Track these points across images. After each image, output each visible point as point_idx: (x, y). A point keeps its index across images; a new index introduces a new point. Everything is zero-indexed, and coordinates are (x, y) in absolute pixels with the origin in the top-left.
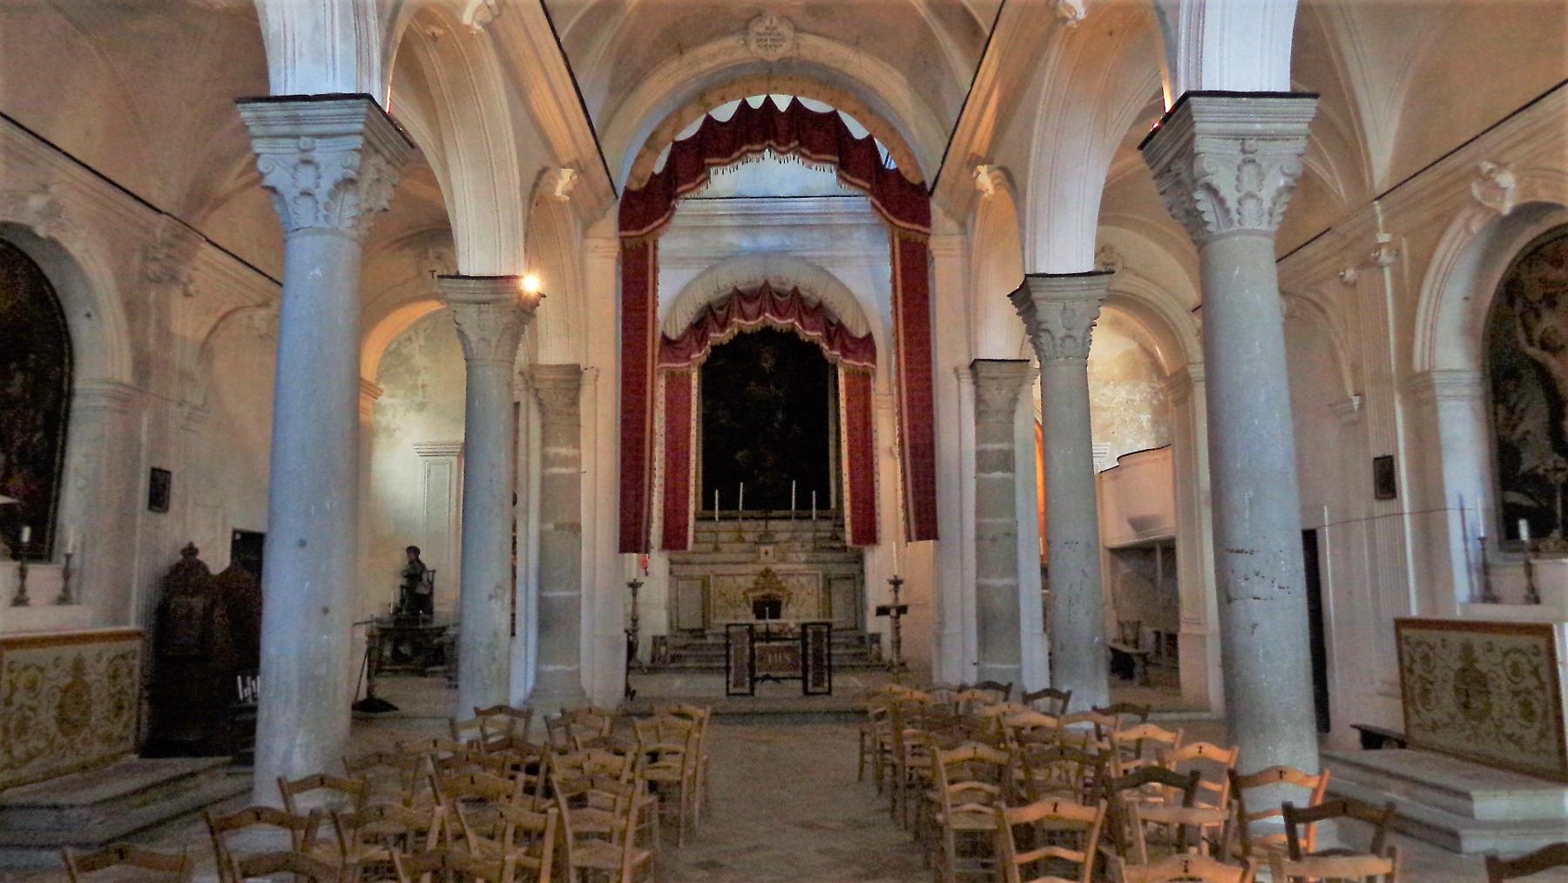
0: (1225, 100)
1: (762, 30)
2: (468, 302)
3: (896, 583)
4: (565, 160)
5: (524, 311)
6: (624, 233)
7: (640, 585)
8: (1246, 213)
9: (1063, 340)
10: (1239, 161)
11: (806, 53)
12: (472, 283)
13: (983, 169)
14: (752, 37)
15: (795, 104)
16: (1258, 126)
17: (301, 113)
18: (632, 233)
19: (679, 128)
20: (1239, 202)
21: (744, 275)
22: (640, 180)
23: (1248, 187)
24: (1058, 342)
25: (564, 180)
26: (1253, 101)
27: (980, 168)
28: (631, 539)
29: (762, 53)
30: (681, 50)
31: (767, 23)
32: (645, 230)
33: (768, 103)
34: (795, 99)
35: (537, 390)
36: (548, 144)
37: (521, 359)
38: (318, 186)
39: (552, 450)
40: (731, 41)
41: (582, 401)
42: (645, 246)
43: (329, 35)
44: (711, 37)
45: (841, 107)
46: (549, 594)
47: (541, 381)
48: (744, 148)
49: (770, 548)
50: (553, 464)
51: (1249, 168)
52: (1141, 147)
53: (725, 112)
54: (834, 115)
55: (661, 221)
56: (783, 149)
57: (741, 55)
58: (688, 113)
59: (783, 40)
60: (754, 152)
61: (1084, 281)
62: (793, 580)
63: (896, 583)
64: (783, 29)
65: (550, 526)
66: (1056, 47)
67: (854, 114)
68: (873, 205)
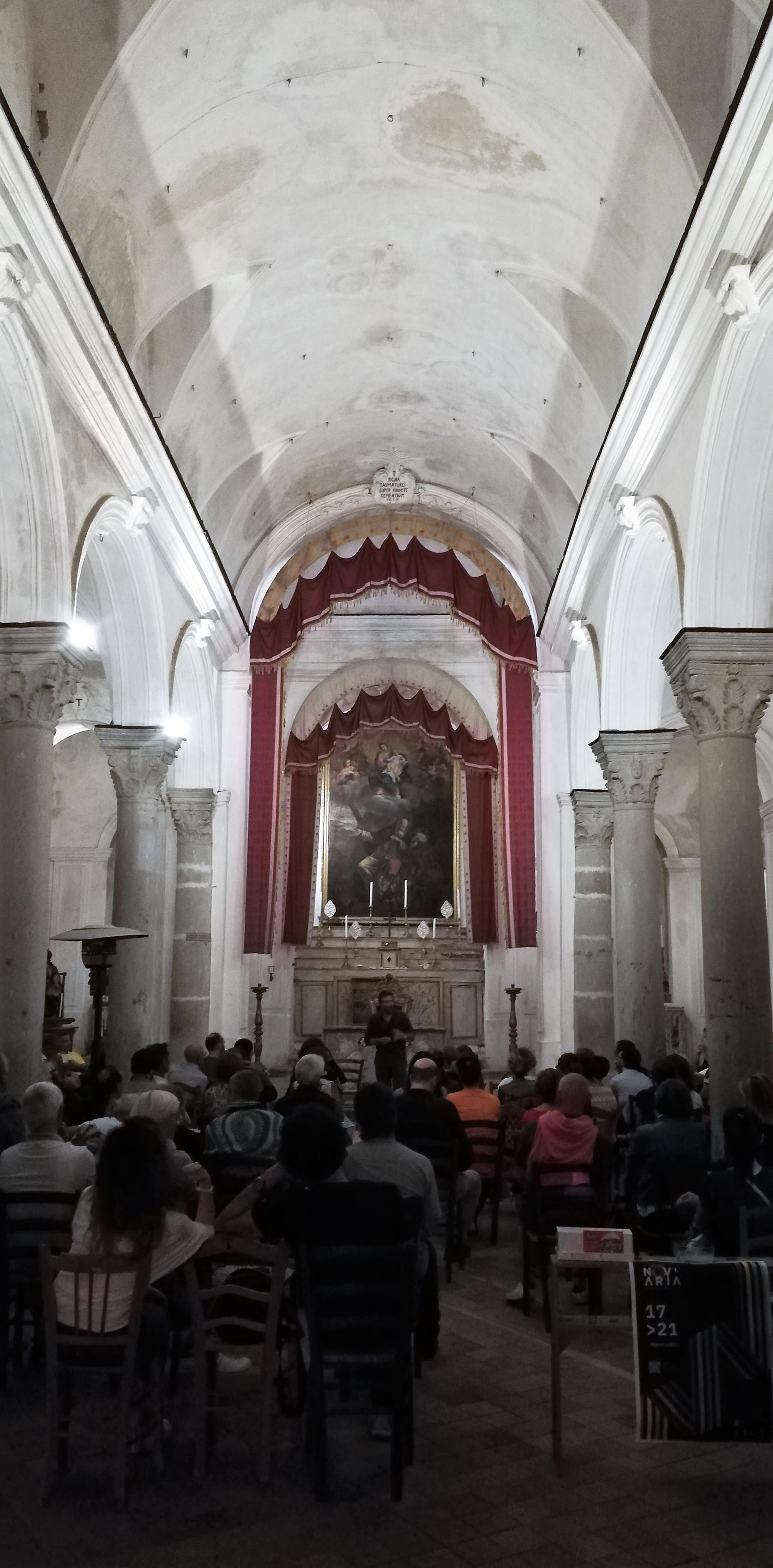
0: (714, 634)
1: (386, 481)
2: (121, 748)
3: (513, 992)
4: (203, 611)
5: (168, 754)
6: (254, 660)
7: (264, 990)
8: (731, 721)
9: (632, 787)
10: (726, 681)
11: (425, 500)
12: (124, 732)
13: (577, 624)
14: (376, 489)
15: (414, 544)
16: (740, 654)
17: (13, 636)
18: (262, 660)
19: (304, 566)
20: (726, 713)
21: (373, 679)
22: (270, 611)
23: (734, 699)
24: (628, 789)
25: (202, 630)
26: (735, 635)
27: (574, 623)
28: (254, 940)
29: (385, 501)
30: (311, 500)
31: (391, 475)
32: (274, 658)
33: (390, 542)
34: (414, 539)
35: (173, 811)
36: (189, 600)
37: (163, 789)
38: (23, 690)
39: (186, 867)
40: (357, 490)
41: (215, 822)
42: (274, 674)
43: (33, 574)
44: (340, 488)
45: (457, 547)
46: (176, 999)
47: (179, 803)
48: (368, 584)
49: (393, 955)
50: (187, 880)
51: (735, 686)
52: (661, 658)
53: (348, 551)
54: (450, 554)
55: (288, 650)
56: (404, 585)
57: (366, 501)
58: (315, 550)
59: (405, 490)
60: (377, 587)
61: (650, 737)
62: (414, 987)
63: (513, 992)
64: (406, 479)
65: (183, 936)
66: (494, 723)
67: (468, 554)
68: (483, 642)
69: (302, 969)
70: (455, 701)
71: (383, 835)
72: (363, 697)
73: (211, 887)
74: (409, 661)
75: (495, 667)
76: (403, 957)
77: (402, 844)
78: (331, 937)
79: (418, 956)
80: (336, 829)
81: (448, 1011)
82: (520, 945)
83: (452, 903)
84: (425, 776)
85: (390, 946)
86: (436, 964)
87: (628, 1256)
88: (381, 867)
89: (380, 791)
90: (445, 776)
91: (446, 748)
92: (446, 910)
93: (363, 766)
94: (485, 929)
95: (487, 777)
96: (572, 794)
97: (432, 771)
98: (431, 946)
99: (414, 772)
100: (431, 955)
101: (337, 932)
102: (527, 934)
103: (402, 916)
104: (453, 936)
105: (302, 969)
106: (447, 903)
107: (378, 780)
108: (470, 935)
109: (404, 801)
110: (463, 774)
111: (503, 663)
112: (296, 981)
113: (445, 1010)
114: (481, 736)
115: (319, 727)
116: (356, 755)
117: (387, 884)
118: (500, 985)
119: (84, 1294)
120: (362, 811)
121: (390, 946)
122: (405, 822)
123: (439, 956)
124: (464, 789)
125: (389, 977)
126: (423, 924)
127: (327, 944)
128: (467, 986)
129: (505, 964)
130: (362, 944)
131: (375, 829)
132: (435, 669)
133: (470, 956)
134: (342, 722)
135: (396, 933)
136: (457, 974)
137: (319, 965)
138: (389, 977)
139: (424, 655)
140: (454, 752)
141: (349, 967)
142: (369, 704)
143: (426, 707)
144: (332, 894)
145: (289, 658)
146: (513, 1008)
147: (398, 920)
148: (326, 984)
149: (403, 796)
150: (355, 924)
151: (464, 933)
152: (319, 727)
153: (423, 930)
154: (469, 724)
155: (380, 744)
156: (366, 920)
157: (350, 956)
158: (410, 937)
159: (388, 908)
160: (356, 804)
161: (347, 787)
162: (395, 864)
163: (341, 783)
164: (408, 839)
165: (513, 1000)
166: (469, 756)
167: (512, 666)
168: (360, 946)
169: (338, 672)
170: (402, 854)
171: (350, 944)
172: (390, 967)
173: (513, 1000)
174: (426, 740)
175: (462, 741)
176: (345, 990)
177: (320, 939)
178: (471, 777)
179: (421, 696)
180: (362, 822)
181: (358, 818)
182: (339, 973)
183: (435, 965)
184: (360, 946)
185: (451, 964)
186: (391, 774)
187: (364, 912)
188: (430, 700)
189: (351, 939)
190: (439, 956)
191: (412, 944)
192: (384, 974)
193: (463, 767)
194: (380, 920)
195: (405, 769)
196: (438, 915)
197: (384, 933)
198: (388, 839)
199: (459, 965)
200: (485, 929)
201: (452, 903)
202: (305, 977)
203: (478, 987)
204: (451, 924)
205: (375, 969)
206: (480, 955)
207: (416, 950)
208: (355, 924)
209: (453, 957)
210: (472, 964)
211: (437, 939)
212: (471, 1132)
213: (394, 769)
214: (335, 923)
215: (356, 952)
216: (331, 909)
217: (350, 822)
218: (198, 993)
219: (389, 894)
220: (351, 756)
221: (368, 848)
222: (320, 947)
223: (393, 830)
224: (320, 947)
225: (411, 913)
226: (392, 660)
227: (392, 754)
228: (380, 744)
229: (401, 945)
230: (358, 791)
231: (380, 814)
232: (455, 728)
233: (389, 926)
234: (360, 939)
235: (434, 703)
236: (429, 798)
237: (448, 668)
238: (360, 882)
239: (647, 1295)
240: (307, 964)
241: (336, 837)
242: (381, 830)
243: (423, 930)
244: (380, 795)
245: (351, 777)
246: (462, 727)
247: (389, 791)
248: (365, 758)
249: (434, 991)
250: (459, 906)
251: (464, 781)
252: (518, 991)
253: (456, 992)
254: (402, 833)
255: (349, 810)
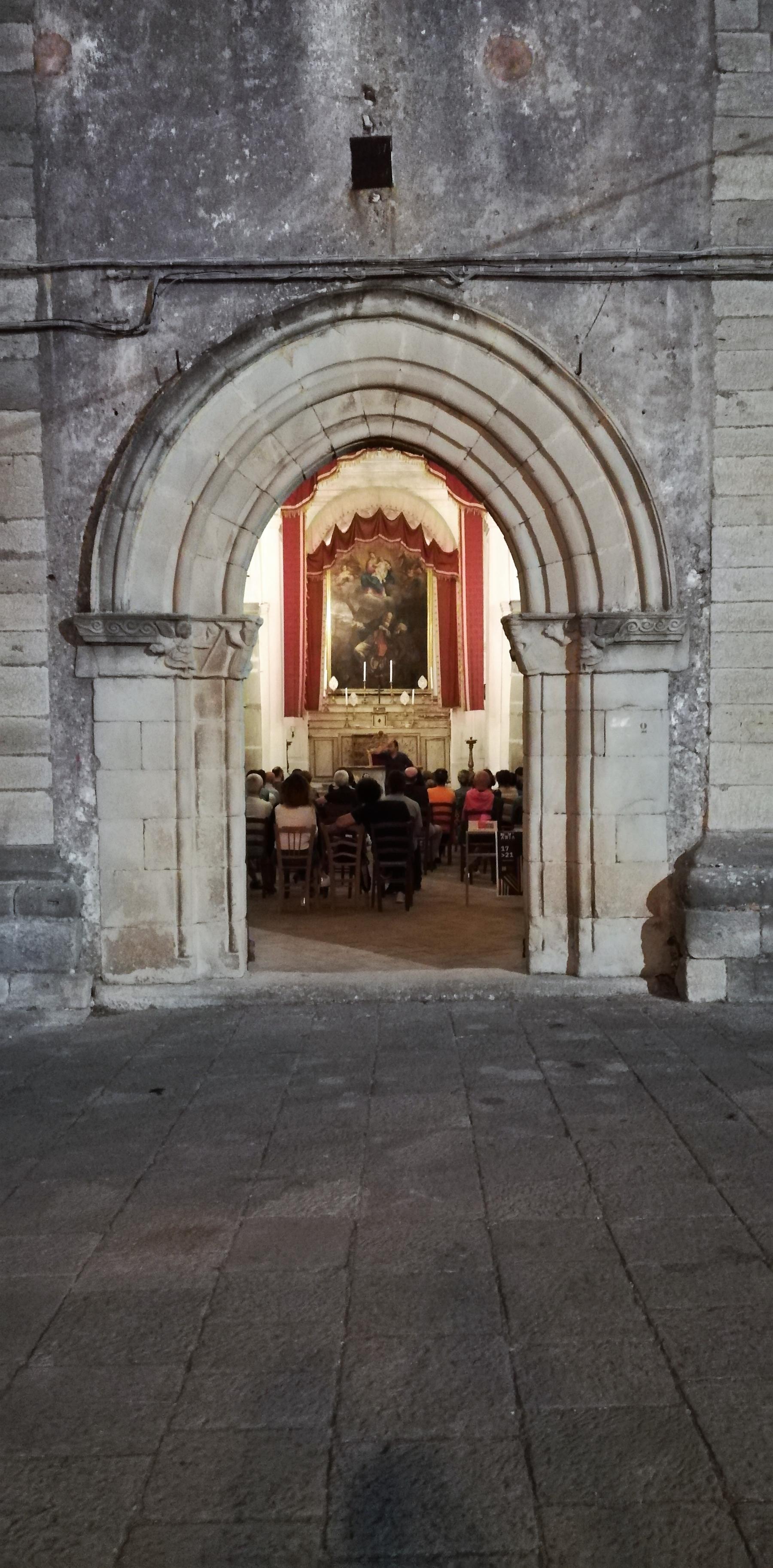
18: (289, 507)
21: (366, 507)
28: (290, 710)
42: (298, 517)
49: (382, 718)
55: (308, 499)
63: (471, 743)
69: (314, 728)
70: (428, 521)
71: (372, 627)
72: (357, 519)
73: (259, 672)
74: (393, 488)
75: (457, 511)
76: (390, 719)
77: (388, 633)
78: (335, 705)
79: (401, 718)
80: (336, 620)
81: (423, 758)
82: (473, 708)
83: (426, 677)
84: (405, 578)
85: (380, 711)
86: (415, 724)
87: (495, 830)
88: (372, 651)
89: (370, 591)
90: (421, 578)
91: (421, 559)
92: (422, 682)
93: (356, 570)
94: (451, 699)
95: (453, 581)
96: (510, 603)
97: (411, 574)
98: (411, 710)
99: (395, 574)
100: (411, 717)
101: (339, 701)
102: (477, 703)
103: (388, 687)
104: (427, 702)
105: (314, 728)
106: (422, 678)
107: (368, 582)
108: (440, 702)
109: (390, 599)
110: (435, 579)
111: (463, 509)
112: (310, 737)
113: (422, 756)
114: (448, 549)
115: (323, 543)
116: (352, 563)
117: (376, 664)
118: (462, 735)
119: (292, 841)
120: (357, 607)
121: (380, 711)
122: (390, 615)
123: (417, 718)
124: (436, 591)
125: (381, 733)
126: (405, 694)
127: (331, 710)
128: (438, 739)
129: (465, 723)
130: (358, 710)
131: (367, 621)
132: (411, 494)
133: (440, 717)
134: (341, 539)
135: (385, 701)
136: (430, 731)
137: (327, 725)
138: (381, 733)
139: (404, 483)
140: (427, 561)
141: (349, 727)
142: (361, 524)
143: (406, 526)
144: (335, 672)
145: (308, 506)
146: (471, 754)
147: (386, 691)
148: (332, 740)
149: (388, 595)
150: (353, 695)
151: (436, 700)
152: (323, 543)
153: (404, 698)
154: (440, 542)
155: (370, 553)
156: (361, 691)
157: (350, 718)
158: (395, 703)
159: (378, 682)
160: (351, 601)
161: (345, 588)
162: (383, 649)
163: (339, 585)
164: (392, 628)
165: (471, 748)
166: (439, 565)
167: (469, 510)
168: (359, 712)
169: (337, 498)
170: (388, 640)
171: (350, 710)
172: (378, 726)
173: (471, 748)
174: (406, 553)
175: (433, 552)
176: (347, 744)
177: (327, 706)
178: (441, 581)
179: (402, 518)
180: (357, 615)
181: (354, 613)
182: (343, 732)
183: (414, 725)
184: (359, 712)
185: (426, 724)
186: (379, 577)
187: (359, 685)
188: (408, 519)
189: (350, 706)
190: (417, 718)
191: (397, 709)
192: (377, 732)
193: (435, 574)
194: (372, 691)
195: (389, 572)
196: (416, 686)
197: (375, 701)
198: (377, 628)
199: (433, 724)
200: (451, 699)
201: (426, 677)
202: (315, 734)
203: (445, 740)
204: (426, 694)
205: (369, 728)
206: (447, 717)
207: (400, 714)
208: (353, 695)
209: (427, 718)
210: (442, 723)
211: (415, 705)
212: (436, 809)
213: (380, 574)
214: (338, 694)
215: (354, 716)
216: (334, 683)
217: (347, 616)
218: (255, 744)
219: (378, 671)
220: (347, 563)
221: (362, 636)
222: (327, 712)
223: (381, 621)
224: (327, 712)
225: (395, 686)
226: (379, 488)
227: (379, 561)
228: (370, 553)
229: (388, 710)
230: (353, 591)
231: (370, 609)
232: (428, 542)
233: (379, 695)
234: (357, 706)
235: (412, 522)
236: (408, 595)
237: (423, 494)
238: (356, 661)
239: (502, 843)
240: (317, 725)
241: (336, 628)
242: (372, 621)
243: (404, 698)
244: (370, 594)
245: (347, 579)
246: (434, 542)
247: (377, 591)
248: (358, 563)
249: (414, 743)
250: (432, 680)
251: (435, 585)
252: (475, 742)
253: (430, 744)
254: (387, 624)
255: (347, 606)
